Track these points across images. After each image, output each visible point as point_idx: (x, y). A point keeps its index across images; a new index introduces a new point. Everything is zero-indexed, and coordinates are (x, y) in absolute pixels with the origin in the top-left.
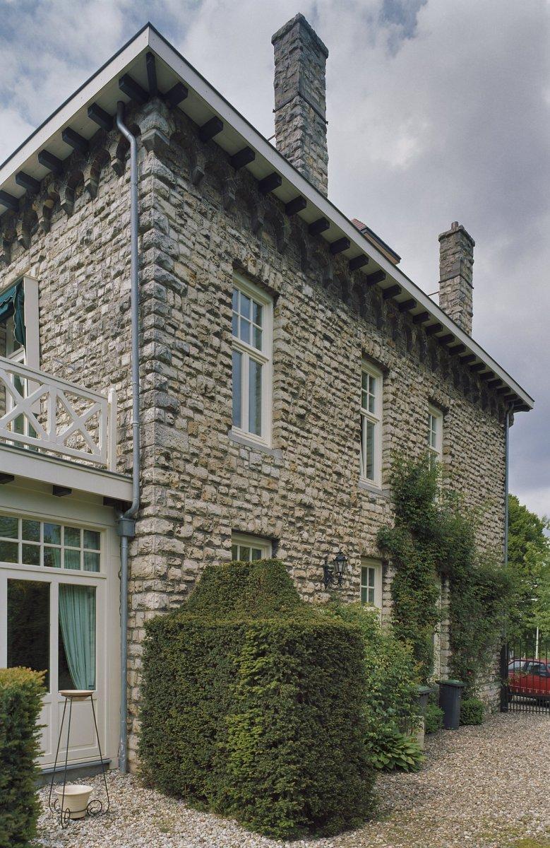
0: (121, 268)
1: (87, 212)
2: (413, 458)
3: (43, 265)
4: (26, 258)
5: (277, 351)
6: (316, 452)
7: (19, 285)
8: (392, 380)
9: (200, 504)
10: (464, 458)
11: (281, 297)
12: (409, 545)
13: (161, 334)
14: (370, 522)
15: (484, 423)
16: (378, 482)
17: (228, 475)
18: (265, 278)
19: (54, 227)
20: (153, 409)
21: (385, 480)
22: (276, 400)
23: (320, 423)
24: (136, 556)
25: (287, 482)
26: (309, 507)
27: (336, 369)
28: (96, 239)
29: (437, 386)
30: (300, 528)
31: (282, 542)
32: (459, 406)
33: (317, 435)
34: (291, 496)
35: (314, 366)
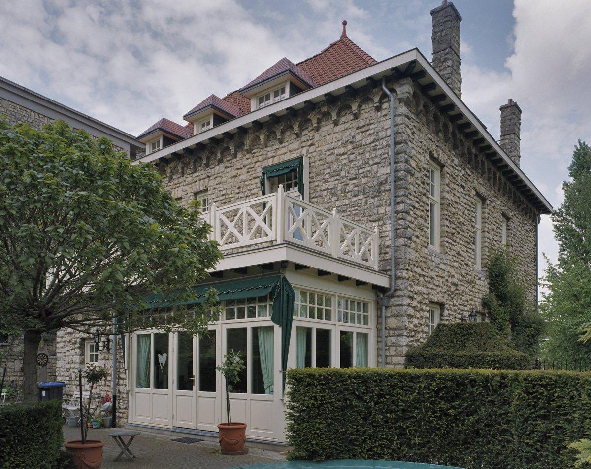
0: (379, 161)
1: (351, 126)
2: (496, 250)
3: (312, 149)
4: (299, 142)
5: (442, 198)
6: (458, 253)
7: (301, 158)
8: (487, 205)
9: (419, 288)
10: (517, 247)
11: (445, 167)
12: (495, 304)
13: (406, 198)
14: (479, 291)
15: (526, 224)
16: (478, 267)
17: (428, 271)
18: (440, 158)
19: (323, 129)
20: (403, 239)
21: (483, 265)
22: (442, 226)
23: (460, 236)
24: (389, 317)
25: (448, 272)
26: (455, 285)
27: (465, 204)
28: (357, 142)
29: (506, 205)
30: (453, 298)
31: (446, 306)
32: (515, 215)
33: (458, 243)
34: (450, 279)
35: (457, 203)
